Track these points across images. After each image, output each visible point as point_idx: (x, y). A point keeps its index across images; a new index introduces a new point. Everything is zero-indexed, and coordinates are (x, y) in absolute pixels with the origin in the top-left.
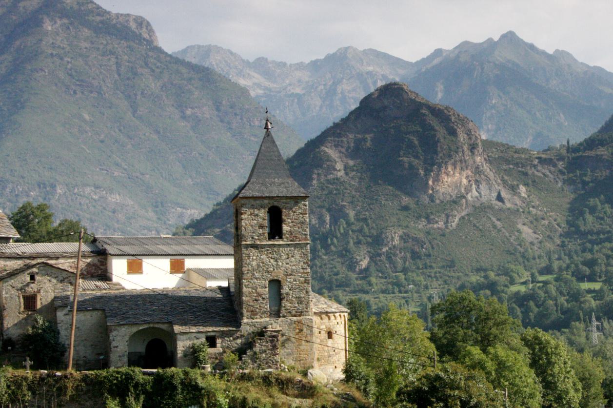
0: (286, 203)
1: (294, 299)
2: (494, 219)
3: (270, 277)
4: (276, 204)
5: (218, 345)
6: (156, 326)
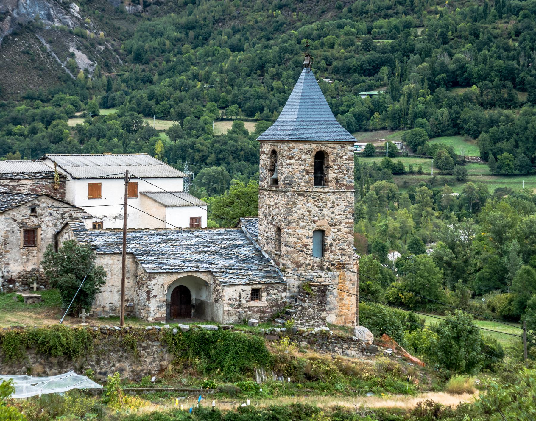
0: (333, 148)
1: (337, 251)
2: (44, 42)
3: (316, 226)
4: (323, 148)
5: (264, 299)
6: (194, 275)
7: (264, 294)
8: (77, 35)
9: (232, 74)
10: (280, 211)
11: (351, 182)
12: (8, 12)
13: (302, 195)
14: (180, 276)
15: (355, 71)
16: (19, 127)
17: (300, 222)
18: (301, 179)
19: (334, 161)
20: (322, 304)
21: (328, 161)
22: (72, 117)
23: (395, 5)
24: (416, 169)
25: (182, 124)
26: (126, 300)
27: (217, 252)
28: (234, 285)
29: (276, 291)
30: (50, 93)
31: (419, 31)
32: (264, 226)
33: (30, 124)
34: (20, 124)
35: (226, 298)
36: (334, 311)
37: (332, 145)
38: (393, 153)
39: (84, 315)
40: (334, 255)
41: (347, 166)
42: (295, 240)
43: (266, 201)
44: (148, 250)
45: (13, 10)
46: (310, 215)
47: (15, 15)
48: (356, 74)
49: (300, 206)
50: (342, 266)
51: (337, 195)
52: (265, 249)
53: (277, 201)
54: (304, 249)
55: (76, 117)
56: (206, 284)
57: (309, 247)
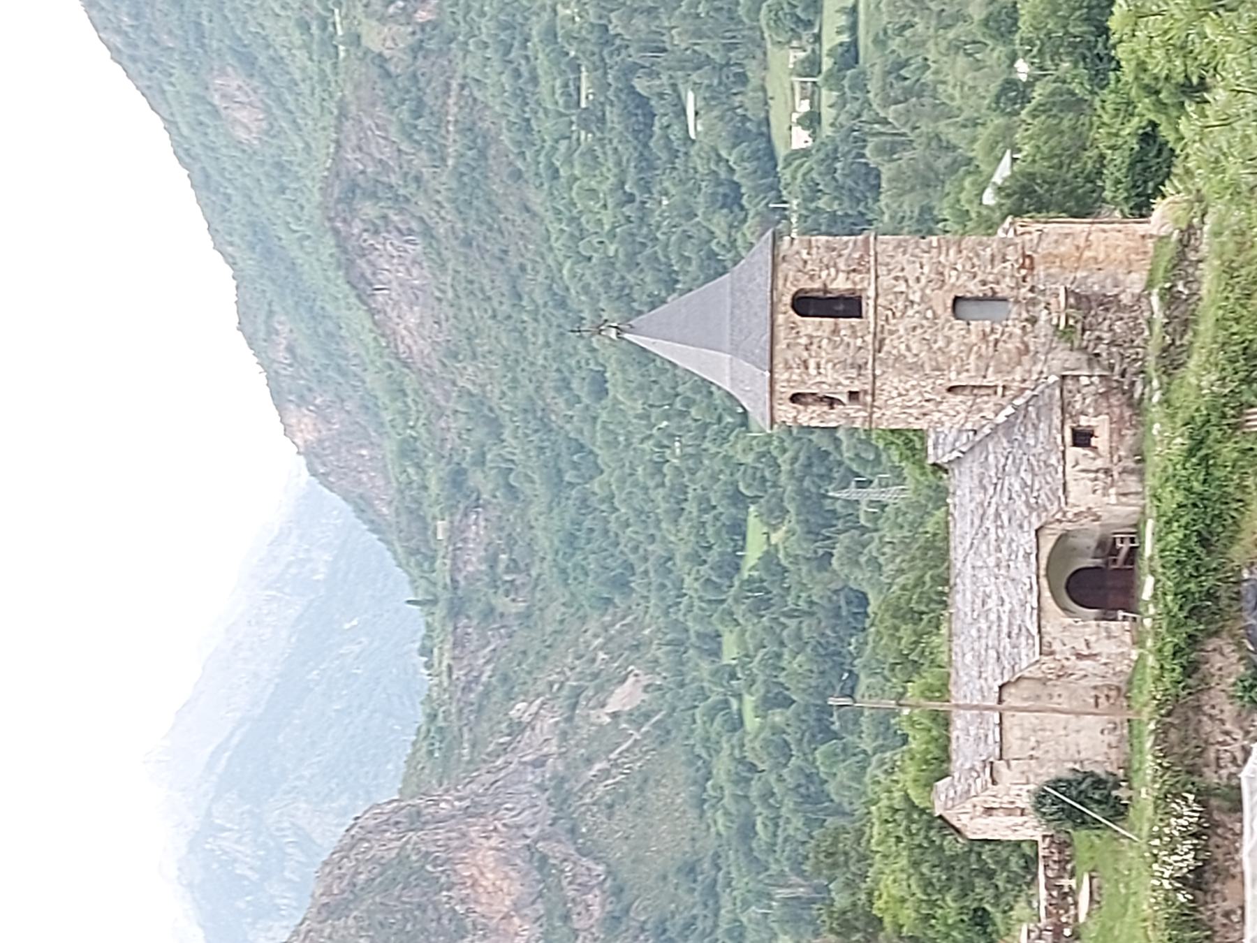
0: (786, 280)
3: (945, 314)
4: (787, 299)
5: (1093, 422)
6: (1043, 563)
7: (1084, 421)
8: (574, 706)
9: (653, 397)
10: (913, 387)
11: (855, 243)
12: (528, 846)
13: (882, 341)
14: (1047, 594)
15: (646, 145)
16: (759, 827)
17: (935, 347)
18: (848, 345)
19: (812, 278)
20: (1107, 303)
21: (812, 290)
22: (742, 723)
23: (511, 62)
24: (843, 20)
25: (755, 499)
26: (1097, 705)
27: (998, 515)
28: (1065, 484)
29: (1078, 397)
30: (690, 763)
31: (563, 12)
32: (944, 418)
33: (755, 807)
34: (754, 826)
35: (1091, 501)
36: (1121, 277)
37: (780, 282)
38: (812, 66)
39: (1122, 793)
40: (1004, 276)
41: (822, 250)
42: (973, 357)
43: (891, 416)
44: (993, 653)
45: (526, 837)
46: (922, 326)
47: (534, 832)
48: (651, 144)
49: (903, 347)
50: (1028, 262)
51: (882, 270)
52: (991, 416)
53: (894, 394)
54: (992, 338)
55: (740, 711)
56: (1063, 538)
57: (988, 330)
